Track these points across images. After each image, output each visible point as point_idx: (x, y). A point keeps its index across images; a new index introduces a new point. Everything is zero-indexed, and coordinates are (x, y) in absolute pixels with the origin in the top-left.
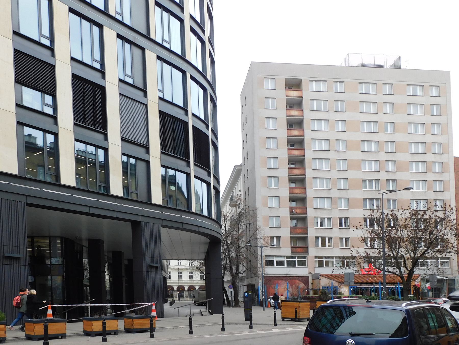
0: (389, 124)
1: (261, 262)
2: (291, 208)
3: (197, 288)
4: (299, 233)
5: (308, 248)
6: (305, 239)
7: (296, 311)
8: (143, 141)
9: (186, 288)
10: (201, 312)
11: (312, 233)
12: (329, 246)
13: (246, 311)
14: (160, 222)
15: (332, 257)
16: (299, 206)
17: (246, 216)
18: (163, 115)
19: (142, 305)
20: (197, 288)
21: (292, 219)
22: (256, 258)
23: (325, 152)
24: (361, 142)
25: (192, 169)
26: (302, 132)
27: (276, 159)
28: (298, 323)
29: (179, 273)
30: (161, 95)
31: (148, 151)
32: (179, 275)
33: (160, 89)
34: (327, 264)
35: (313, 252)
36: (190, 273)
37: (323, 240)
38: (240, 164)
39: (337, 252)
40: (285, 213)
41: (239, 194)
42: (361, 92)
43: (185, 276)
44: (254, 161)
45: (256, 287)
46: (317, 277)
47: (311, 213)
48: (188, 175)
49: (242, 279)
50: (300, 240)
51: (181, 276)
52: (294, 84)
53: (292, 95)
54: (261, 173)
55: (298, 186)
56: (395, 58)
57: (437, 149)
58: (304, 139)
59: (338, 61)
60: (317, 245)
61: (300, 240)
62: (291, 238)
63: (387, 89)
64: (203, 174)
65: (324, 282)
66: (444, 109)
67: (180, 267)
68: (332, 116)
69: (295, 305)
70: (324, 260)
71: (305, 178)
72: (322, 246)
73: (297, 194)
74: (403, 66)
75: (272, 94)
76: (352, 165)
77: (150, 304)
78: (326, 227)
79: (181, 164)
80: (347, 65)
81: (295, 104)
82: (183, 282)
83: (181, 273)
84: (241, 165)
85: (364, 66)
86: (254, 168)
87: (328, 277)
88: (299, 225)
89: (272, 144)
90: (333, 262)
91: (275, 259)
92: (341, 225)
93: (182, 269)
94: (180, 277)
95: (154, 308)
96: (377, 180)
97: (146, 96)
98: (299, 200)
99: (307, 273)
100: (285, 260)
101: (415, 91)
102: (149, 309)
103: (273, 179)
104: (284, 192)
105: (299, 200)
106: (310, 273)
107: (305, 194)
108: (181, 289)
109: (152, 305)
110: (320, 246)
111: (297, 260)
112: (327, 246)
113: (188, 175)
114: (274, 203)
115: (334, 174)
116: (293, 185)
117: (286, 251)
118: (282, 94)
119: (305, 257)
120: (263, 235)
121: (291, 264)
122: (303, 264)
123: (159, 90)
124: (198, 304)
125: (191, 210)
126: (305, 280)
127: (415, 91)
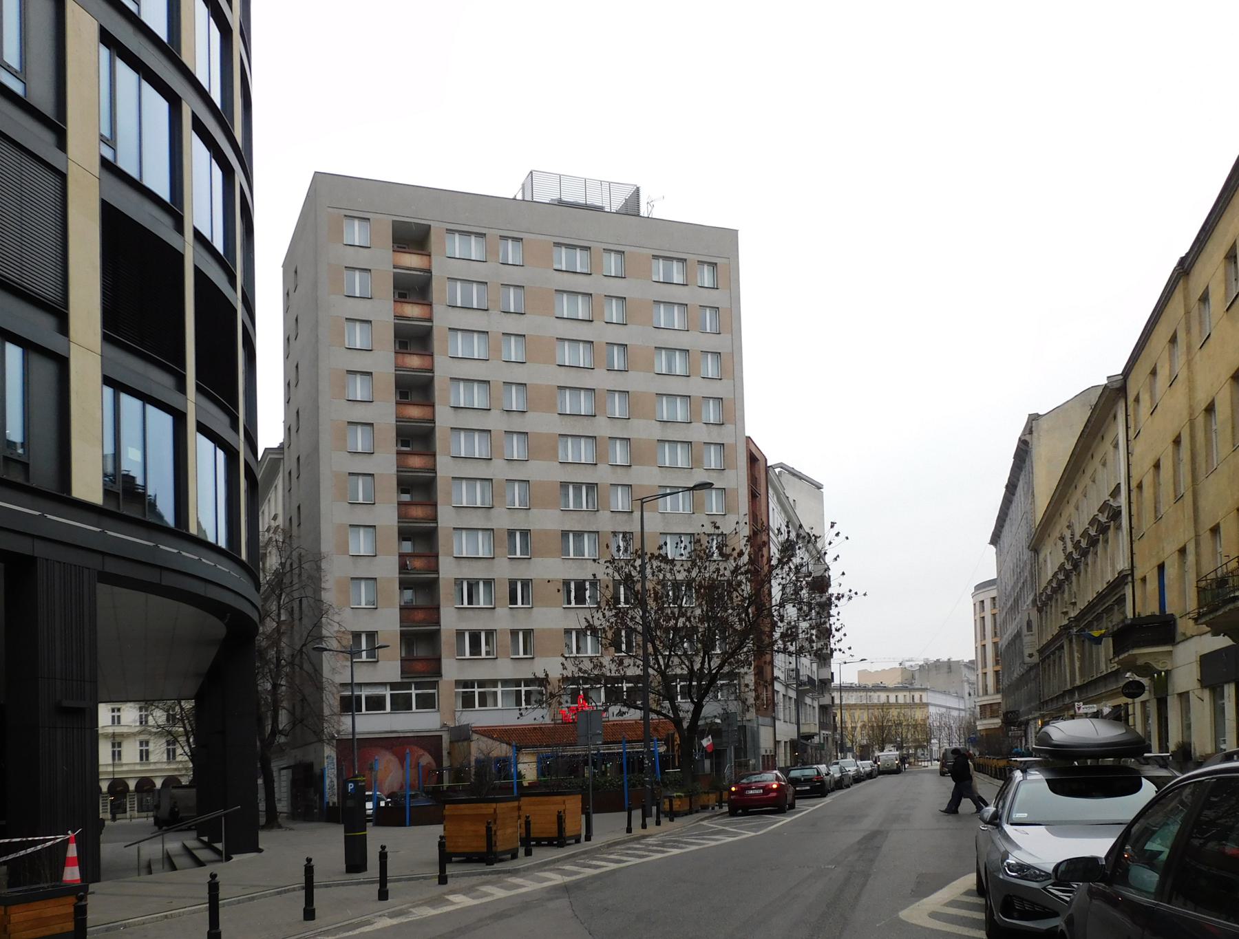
0: (616, 348)
1: (331, 702)
2: (401, 556)
3: (158, 783)
4: (419, 623)
5: (439, 660)
6: (433, 637)
7: (489, 829)
8: (49, 291)
9: (132, 785)
10: (185, 846)
11: (450, 620)
12: (488, 653)
13: (348, 840)
14: (94, 562)
15: (494, 683)
16: (419, 550)
17: (303, 572)
18: (111, 218)
19: (35, 843)
20: (158, 783)
21: (404, 585)
22: (319, 688)
23: (480, 413)
24: (350, 530)
25: (192, 402)
26: (427, 360)
27: (368, 428)
28: (497, 866)
29: (113, 746)
30: (108, 154)
31: (63, 327)
32: (114, 752)
33: (106, 133)
34: (483, 703)
35: (452, 670)
36: (141, 744)
37: (475, 637)
38: (276, 445)
39: (505, 669)
40: (387, 569)
41: (273, 524)
42: (556, 267)
43: (131, 752)
44: (316, 431)
45: (317, 769)
46: (462, 735)
47: (448, 570)
48: (179, 419)
49: (281, 750)
50: (421, 640)
51: (120, 752)
52: (411, 238)
53: (409, 265)
54: (333, 463)
55: (417, 499)
56: (627, 193)
57: (711, 413)
58: (433, 378)
59: (507, 187)
60: (461, 651)
61: (421, 640)
62: (403, 634)
63: (612, 264)
64: (219, 421)
65: (478, 747)
66: (726, 318)
67: (118, 730)
68: (497, 323)
69: (484, 811)
70: (477, 690)
71: (434, 479)
72: (471, 654)
73: (417, 520)
74: (644, 212)
75: (362, 258)
76: (539, 447)
77: (60, 838)
78: (482, 605)
79: (158, 382)
80: (528, 198)
81: (413, 288)
82: (125, 768)
83: (120, 745)
84: (281, 448)
85: (561, 203)
86: (316, 449)
87: (488, 733)
88: (421, 602)
89: (359, 389)
90: (495, 693)
91: (364, 693)
92: (513, 600)
93: (122, 735)
94: (117, 755)
95: (72, 851)
96: (591, 487)
97: (62, 144)
98: (420, 536)
99: (437, 725)
100: (387, 693)
101: (668, 272)
102: (56, 857)
103: (361, 481)
104: (387, 516)
105: (420, 536)
106: (444, 725)
107: (435, 520)
108: (118, 786)
109: (65, 843)
110: (468, 655)
111: (414, 692)
112: (483, 655)
113: (179, 419)
114: (361, 544)
115: (498, 470)
116: (406, 498)
117: (389, 669)
118: (386, 261)
119: (434, 685)
120: (336, 627)
121: (401, 704)
122: (427, 702)
123: (103, 139)
124: (168, 822)
125: (187, 529)
126: (430, 743)
127: (668, 272)
